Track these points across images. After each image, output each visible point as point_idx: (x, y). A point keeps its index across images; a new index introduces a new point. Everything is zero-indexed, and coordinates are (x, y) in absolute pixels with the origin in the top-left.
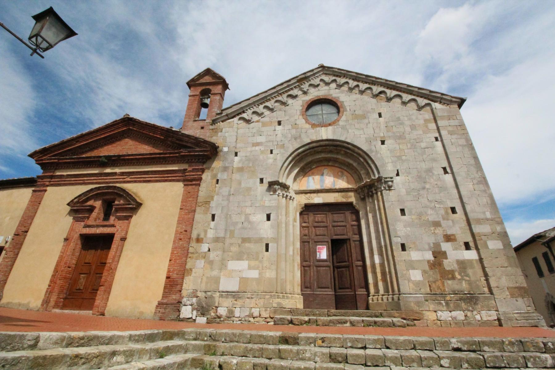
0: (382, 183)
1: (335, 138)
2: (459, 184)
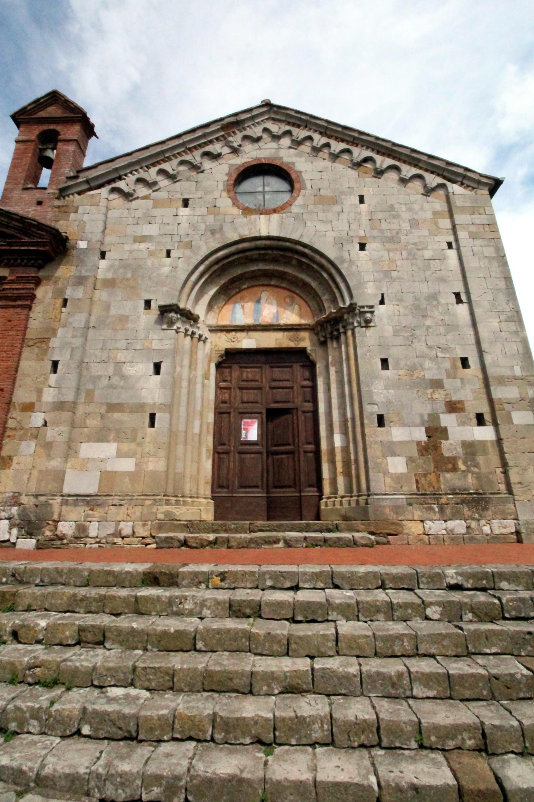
0: (356, 315)
1: (282, 235)
2: (477, 319)
